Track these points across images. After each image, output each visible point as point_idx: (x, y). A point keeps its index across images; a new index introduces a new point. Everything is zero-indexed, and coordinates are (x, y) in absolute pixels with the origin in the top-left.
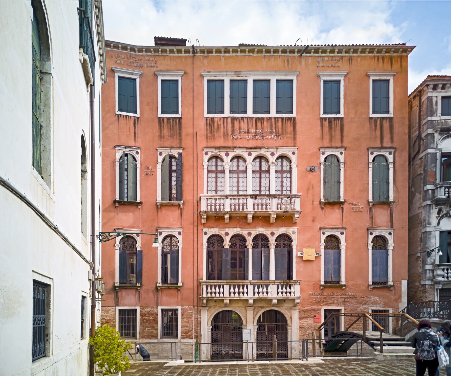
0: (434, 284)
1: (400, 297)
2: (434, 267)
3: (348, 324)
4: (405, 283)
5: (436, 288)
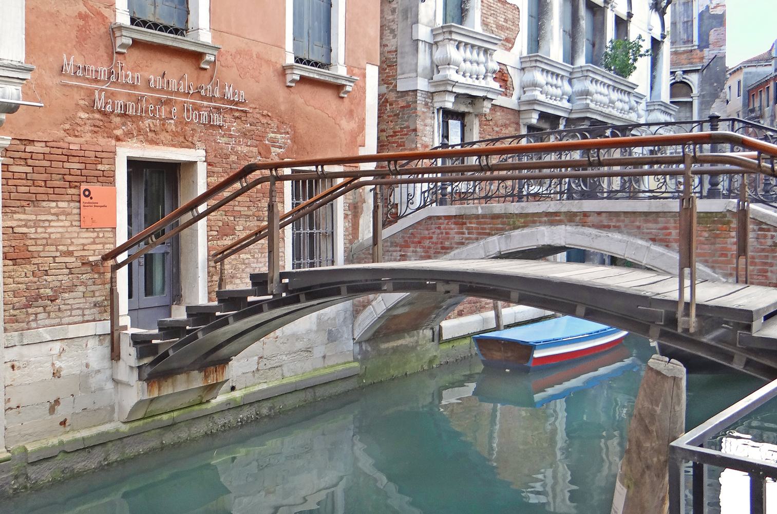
2: (435, 36)
4: (372, 73)
5: (437, 105)
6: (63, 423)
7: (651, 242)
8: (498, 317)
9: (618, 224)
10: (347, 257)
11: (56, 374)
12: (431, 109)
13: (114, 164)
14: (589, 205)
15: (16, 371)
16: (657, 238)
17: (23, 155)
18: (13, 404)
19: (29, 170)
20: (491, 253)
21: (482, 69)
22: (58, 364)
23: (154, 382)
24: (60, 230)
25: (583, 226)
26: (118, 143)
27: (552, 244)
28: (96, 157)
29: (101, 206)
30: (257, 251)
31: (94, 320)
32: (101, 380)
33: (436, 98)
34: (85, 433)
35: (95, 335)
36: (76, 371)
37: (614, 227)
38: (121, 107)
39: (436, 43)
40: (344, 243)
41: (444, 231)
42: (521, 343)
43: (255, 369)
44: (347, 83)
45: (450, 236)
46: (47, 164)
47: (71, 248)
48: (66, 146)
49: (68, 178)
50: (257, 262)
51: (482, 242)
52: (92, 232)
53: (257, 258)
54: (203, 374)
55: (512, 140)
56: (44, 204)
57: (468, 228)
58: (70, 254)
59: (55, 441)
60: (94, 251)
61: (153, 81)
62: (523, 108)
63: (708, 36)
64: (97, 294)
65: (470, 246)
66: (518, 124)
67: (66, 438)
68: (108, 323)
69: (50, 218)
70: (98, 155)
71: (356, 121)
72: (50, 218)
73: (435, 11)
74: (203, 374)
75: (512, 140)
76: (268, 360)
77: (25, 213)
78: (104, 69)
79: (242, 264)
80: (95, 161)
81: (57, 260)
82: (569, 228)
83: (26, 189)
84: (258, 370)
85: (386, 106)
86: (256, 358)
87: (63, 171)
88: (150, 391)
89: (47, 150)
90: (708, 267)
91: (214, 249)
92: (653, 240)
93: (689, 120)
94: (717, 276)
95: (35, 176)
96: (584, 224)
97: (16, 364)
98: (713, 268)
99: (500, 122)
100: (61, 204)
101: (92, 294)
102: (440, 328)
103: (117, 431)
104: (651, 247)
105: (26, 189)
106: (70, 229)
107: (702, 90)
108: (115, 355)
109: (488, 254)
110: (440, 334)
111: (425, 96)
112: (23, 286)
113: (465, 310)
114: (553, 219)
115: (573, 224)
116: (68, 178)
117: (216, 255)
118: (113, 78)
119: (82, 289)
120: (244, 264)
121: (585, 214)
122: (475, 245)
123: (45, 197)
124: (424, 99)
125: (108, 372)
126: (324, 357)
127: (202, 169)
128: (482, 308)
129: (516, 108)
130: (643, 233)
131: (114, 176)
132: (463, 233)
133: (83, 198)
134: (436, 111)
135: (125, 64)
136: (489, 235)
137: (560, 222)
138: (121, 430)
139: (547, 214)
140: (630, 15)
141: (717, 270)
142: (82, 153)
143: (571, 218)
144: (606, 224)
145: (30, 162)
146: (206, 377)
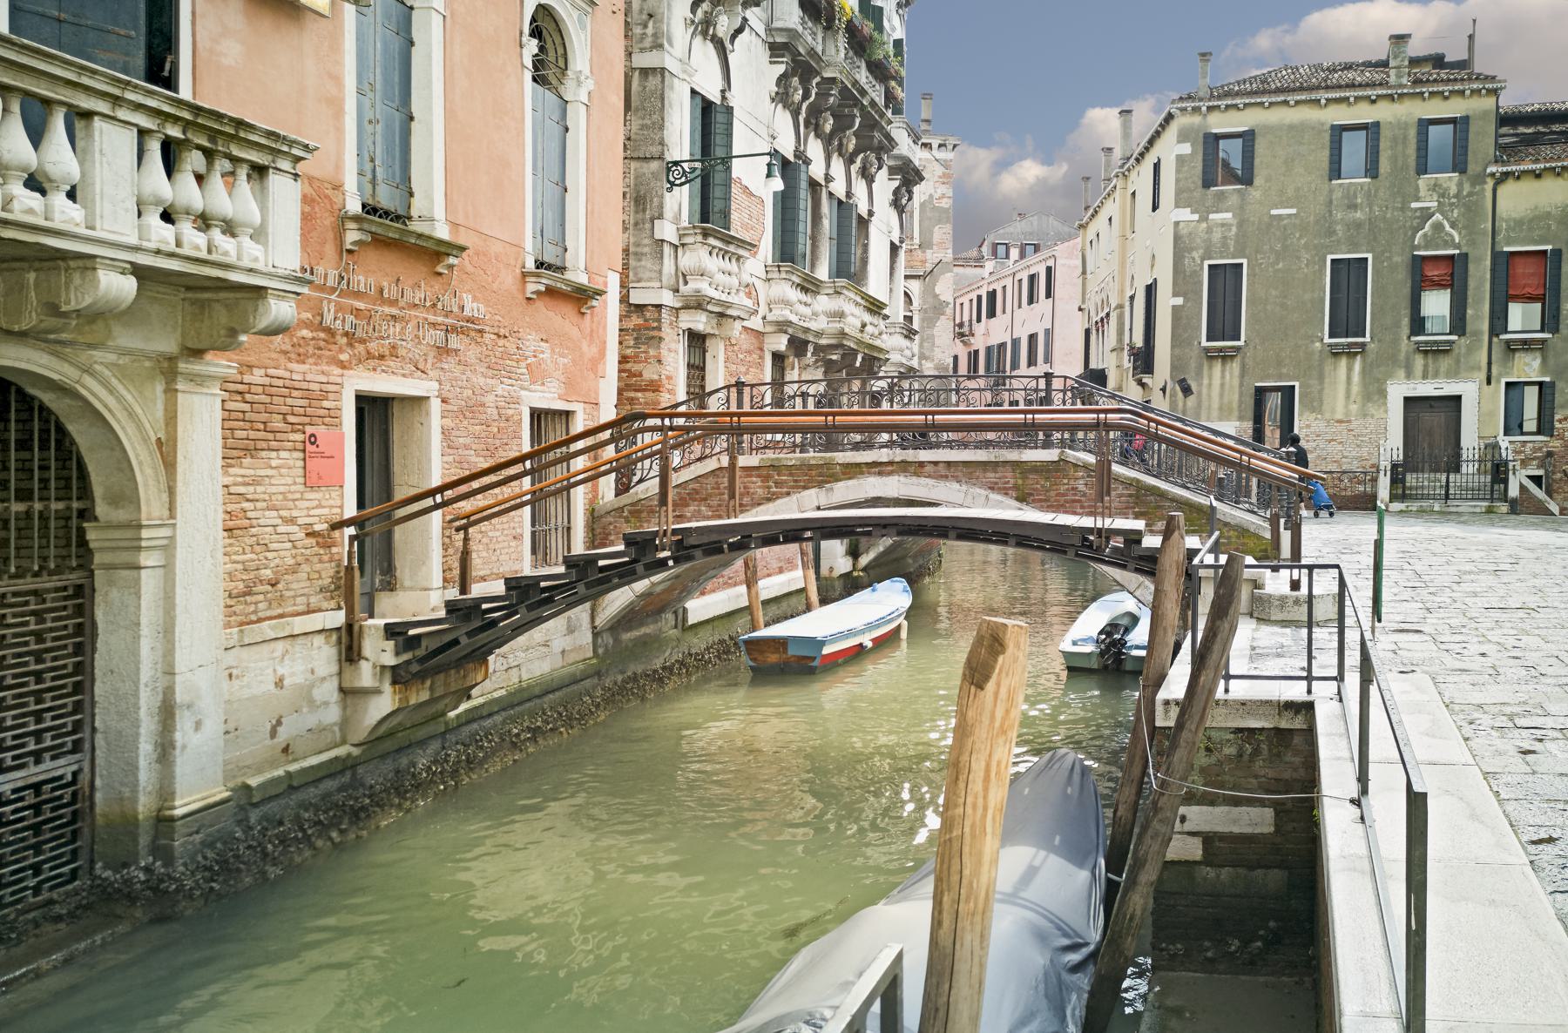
2: (681, 237)
5: (685, 326)
6: (286, 750)
11: (279, 683)
14: (925, 455)
15: (235, 682)
17: (240, 387)
18: (231, 727)
19: (247, 407)
21: (734, 281)
22: (280, 671)
24: (282, 489)
32: (328, 691)
34: (314, 761)
36: (299, 679)
39: (683, 245)
46: (268, 399)
47: (295, 513)
48: (287, 374)
49: (291, 419)
51: (794, 497)
56: (264, 454)
58: (291, 521)
59: (280, 772)
63: (932, 233)
66: (762, 349)
67: (293, 767)
68: (342, 613)
69: (270, 472)
70: (325, 387)
72: (270, 472)
73: (891, 274)
77: (241, 467)
78: (333, 275)
81: (280, 530)
82: (902, 479)
83: (243, 434)
87: (284, 409)
89: (267, 381)
92: (992, 488)
95: (254, 416)
96: (916, 474)
97: (235, 672)
99: (744, 347)
100: (283, 454)
102: (685, 610)
103: (349, 755)
105: (243, 434)
106: (293, 488)
107: (925, 302)
110: (685, 619)
112: (240, 567)
114: (878, 468)
116: (291, 419)
117: (451, 521)
118: (344, 285)
119: (306, 568)
121: (921, 464)
123: (264, 445)
126: (563, 652)
127: (435, 406)
133: (309, 448)
136: (805, 488)
137: (890, 473)
139: (875, 464)
140: (871, 213)
142: (305, 385)
143: (904, 467)
145: (248, 397)
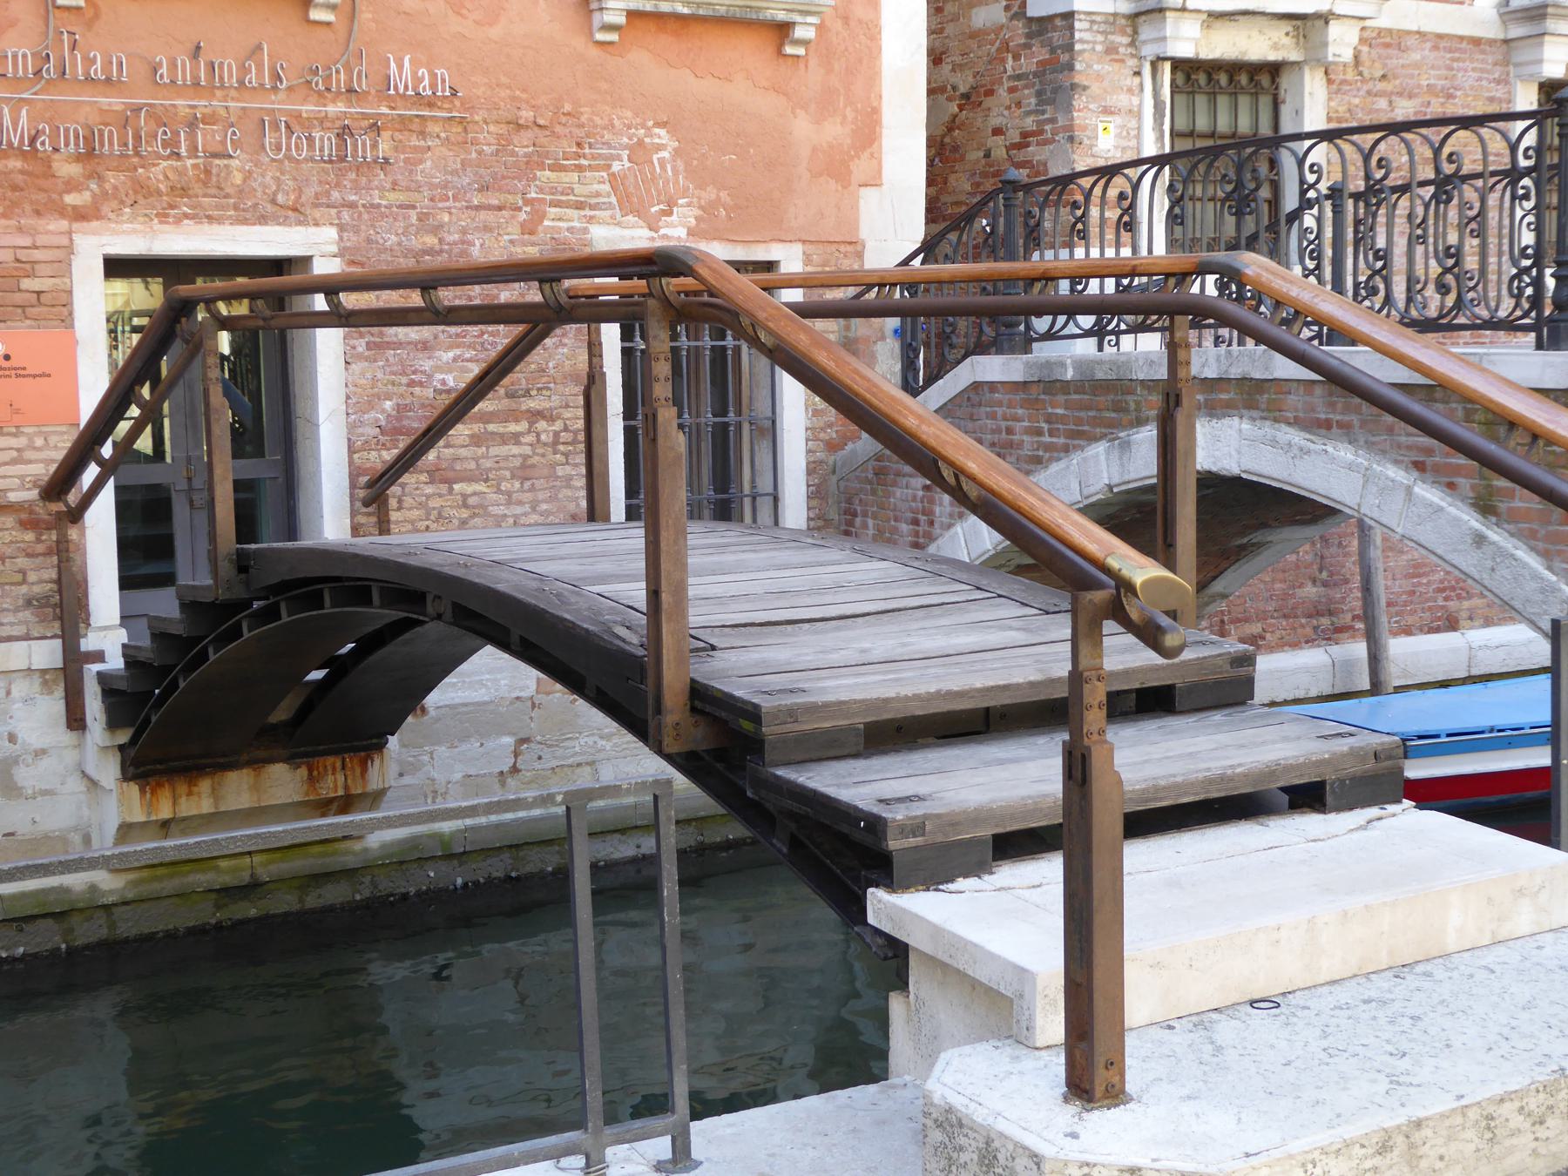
0: (1135, 16)
1: (868, 132)
3: (390, 431)
5: (1149, 51)
7: (1416, 474)
8: (1375, 659)
9: (1347, 418)
10: (818, 486)
12: (1132, 62)
13: (68, 272)
16: (1429, 461)
20: (1092, 490)
23: (160, 785)
25: (1276, 420)
26: (76, 226)
27: (1214, 469)
28: (18, 261)
29: (35, 376)
30: (508, 474)
31: (27, 638)
33: (1146, 32)
35: (29, 669)
37: (1340, 425)
38: (77, 137)
40: (809, 451)
41: (1004, 424)
42: (931, 740)
43: (506, 769)
44: (797, 18)
45: (1016, 438)
50: (509, 503)
51: (1076, 458)
52: (15, 435)
53: (509, 494)
54: (303, 771)
55: (1447, 130)
57: (1049, 419)
60: (22, 477)
61: (164, 70)
62: (1516, 31)
64: (32, 577)
65: (1055, 467)
70: (22, 255)
71: (845, 117)
74: (303, 771)
75: (1378, 135)
76: (550, 746)
79: (459, 507)
80: (16, 269)
84: (515, 770)
85: (1003, 61)
86: (508, 740)
88: (150, 807)
90: (1538, 553)
91: (364, 472)
93: (1504, 109)
94: (1554, 578)
98: (1546, 555)
101: (19, 577)
104: (1416, 489)
108: (75, 720)
109: (1086, 492)
111: (1103, 27)
113: (1268, 636)
115: (1255, 413)
120: (465, 505)
122: (1062, 464)
124: (1100, 38)
125: (71, 757)
128: (1339, 630)
129: (1493, 31)
130: (1399, 446)
131: (68, 304)
132: (1039, 433)
134: (1147, 70)
135: (83, 36)
138: (105, 886)
141: (1557, 564)
144: (1323, 416)
146: (312, 780)
